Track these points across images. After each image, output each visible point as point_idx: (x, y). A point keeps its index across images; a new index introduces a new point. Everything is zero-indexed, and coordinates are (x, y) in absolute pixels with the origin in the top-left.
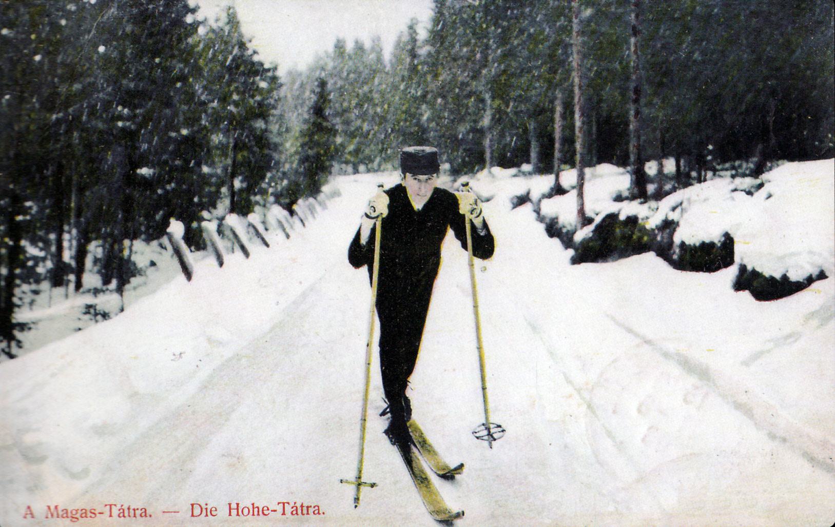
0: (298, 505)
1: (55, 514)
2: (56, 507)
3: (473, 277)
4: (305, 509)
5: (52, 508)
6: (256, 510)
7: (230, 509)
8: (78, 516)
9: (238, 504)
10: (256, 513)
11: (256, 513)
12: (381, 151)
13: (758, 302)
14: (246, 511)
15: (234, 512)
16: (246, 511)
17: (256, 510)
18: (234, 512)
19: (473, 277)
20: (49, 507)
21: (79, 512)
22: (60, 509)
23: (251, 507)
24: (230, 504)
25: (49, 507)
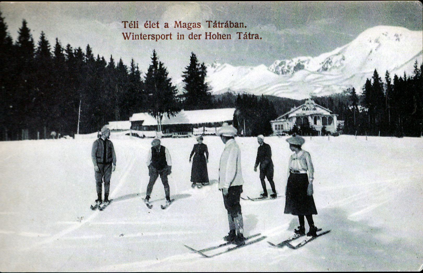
0: (247, 34)
1: (179, 26)
2: (180, 22)
3: (208, 135)
4: (251, 36)
5: (178, 23)
6: (219, 36)
7: (206, 35)
8: (191, 26)
9: (210, 33)
10: (219, 38)
11: (219, 38)
12: (401, 131)
13: (257, 148)
14: (214, 37)
15: (208, 37)
16: (214, 37)
17: (219, 36)
18: (208, 37)
19: (208, 135)
20: (176, 22)
21: (192, 25)
22: (182, 23)
23: (217, 34)
24: (206, 33)
25: (176, 22)
